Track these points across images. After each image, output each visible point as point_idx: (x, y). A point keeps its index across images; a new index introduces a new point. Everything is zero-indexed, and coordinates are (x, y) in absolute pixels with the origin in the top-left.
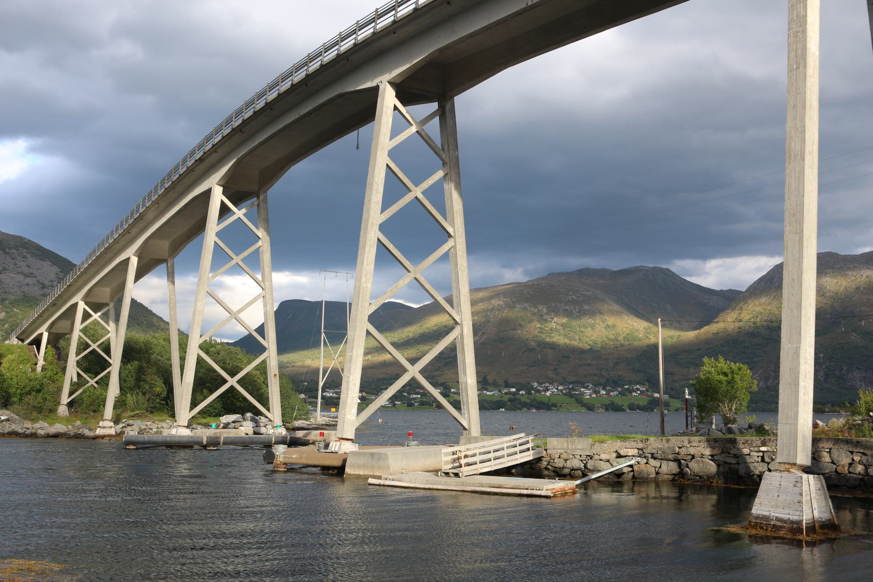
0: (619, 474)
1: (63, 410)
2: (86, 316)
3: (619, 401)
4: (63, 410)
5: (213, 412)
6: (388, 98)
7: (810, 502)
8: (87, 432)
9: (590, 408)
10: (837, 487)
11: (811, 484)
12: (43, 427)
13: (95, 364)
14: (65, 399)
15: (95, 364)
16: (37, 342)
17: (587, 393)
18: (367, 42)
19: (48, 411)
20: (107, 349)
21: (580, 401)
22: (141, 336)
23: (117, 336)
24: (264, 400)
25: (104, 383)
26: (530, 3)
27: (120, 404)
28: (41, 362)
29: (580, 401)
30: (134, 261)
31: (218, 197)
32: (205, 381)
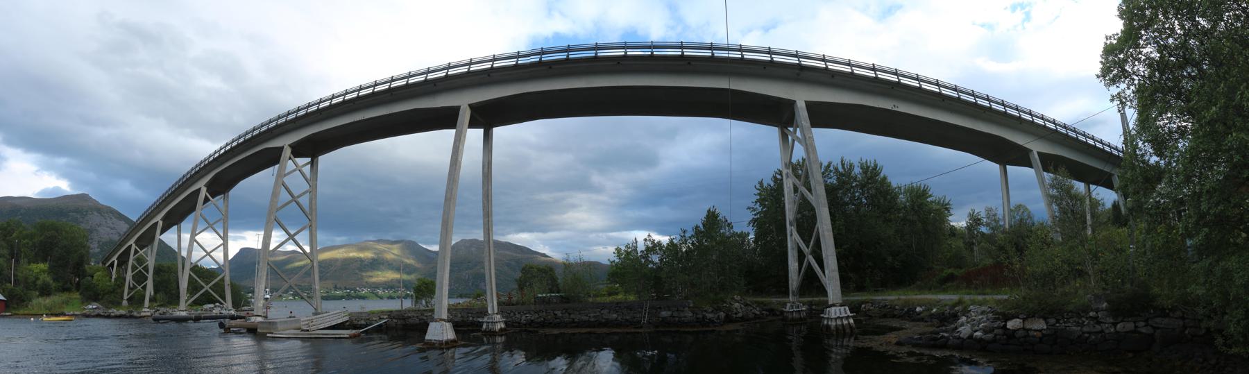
0: (380, 326)
1: (125, 303)
2: (136, 252)
3: (394, 295)
4: (125, 303)
5: (198, 303)
6: (287, 152)
7: (448, 333)
8: (135, 314)
9: (381, 298)
10: (457, 327)
11: (448, 326)
12: (114, 311)
13: (140, 278)
14: (126, 297)
15: (140, 278)
16: (112, 265)
17: (380, 292)
18: (282, 125)
19: (118, 304)
20: (147, 270)
21: (377, 295)
22: (166, 263)
23: (151, 263)
24: (224, 298)
25: (144, 288)
26: (560, 363)
27: (152, 300)
28: (114, 277)
29: (377, 295)
30: (161, 223)
31: (204, 192)
32: (193, 287)
